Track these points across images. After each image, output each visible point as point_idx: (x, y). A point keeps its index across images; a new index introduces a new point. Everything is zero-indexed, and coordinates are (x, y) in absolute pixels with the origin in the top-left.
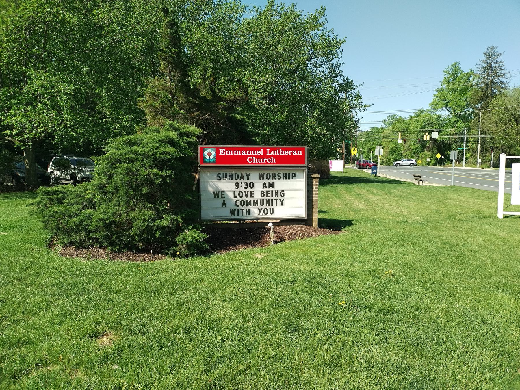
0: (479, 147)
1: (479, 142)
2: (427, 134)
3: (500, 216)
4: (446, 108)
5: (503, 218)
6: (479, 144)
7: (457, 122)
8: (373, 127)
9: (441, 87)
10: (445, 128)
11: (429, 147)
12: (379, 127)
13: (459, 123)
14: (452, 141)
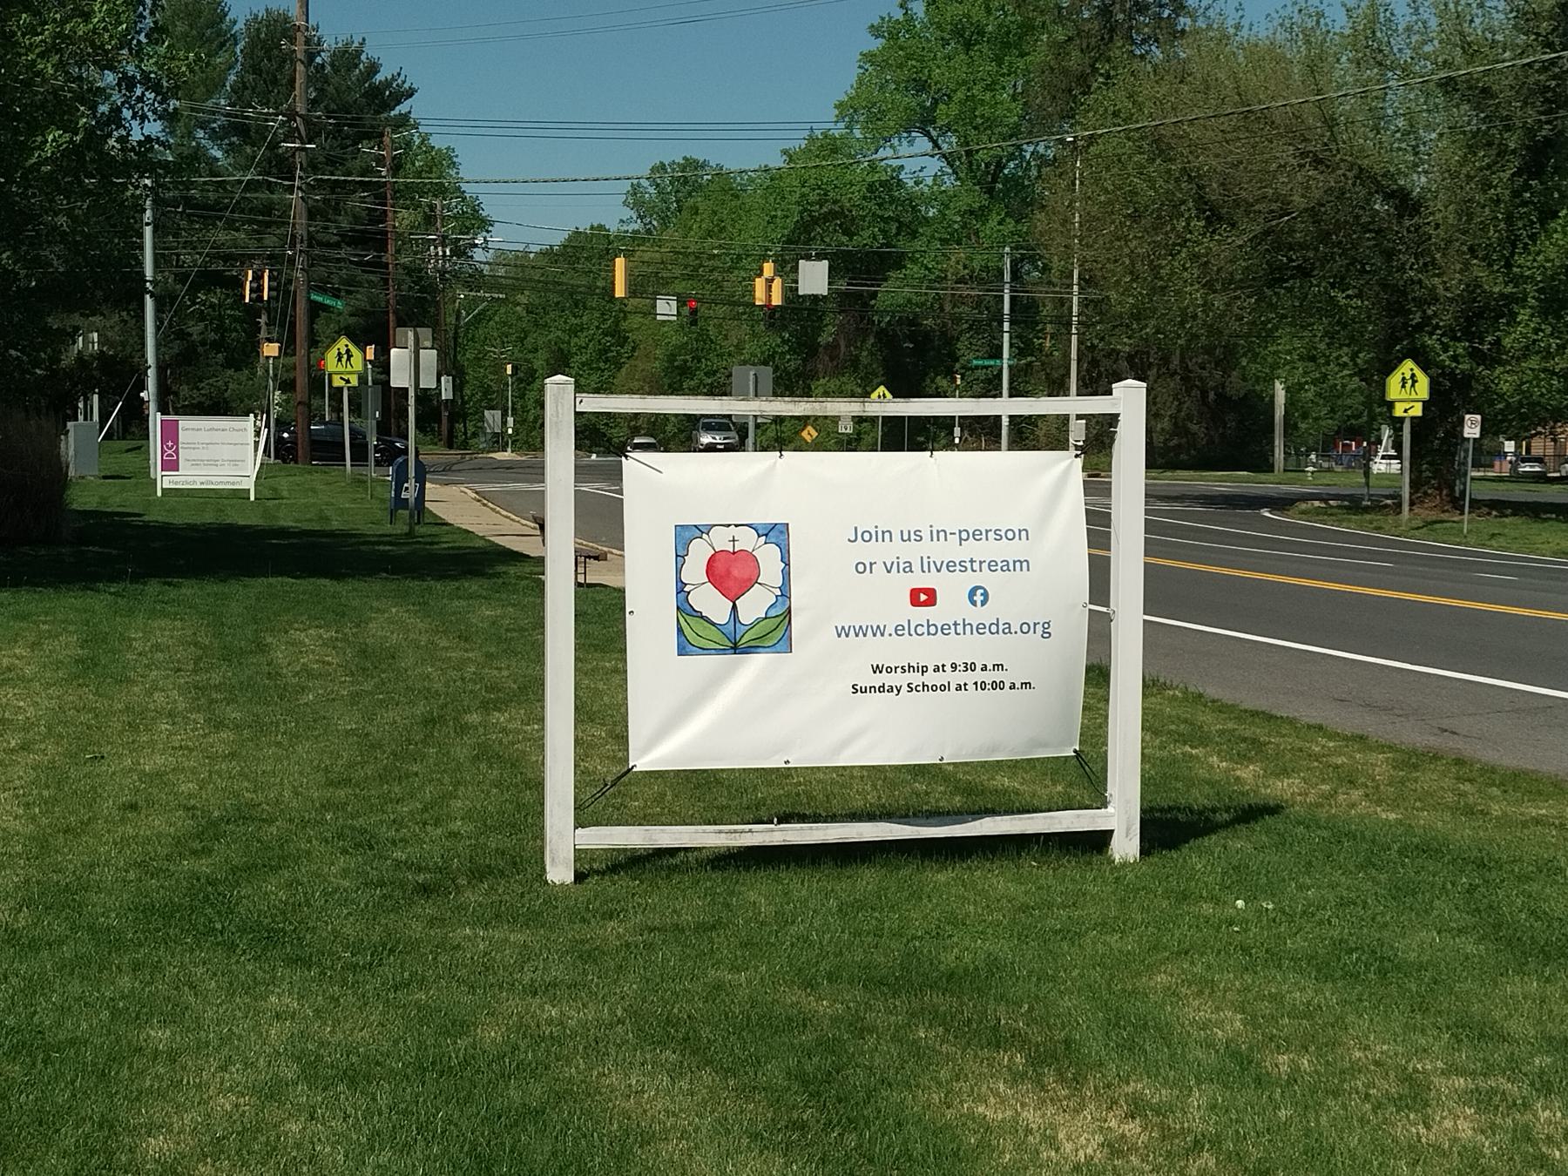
0: (1074, 355)
1: (1006, 326)
2: (768, 268)
3: (560, 872)
4: (928, 134)
5: (580, 877)
6: (1074, 339)
7: (981, 214)
8: (584, 227)
9: (899, 15)
10: (918, 244)
11: (833, 347)
12: (613, 227)
13: (993, 222)
14: (957, 320)
